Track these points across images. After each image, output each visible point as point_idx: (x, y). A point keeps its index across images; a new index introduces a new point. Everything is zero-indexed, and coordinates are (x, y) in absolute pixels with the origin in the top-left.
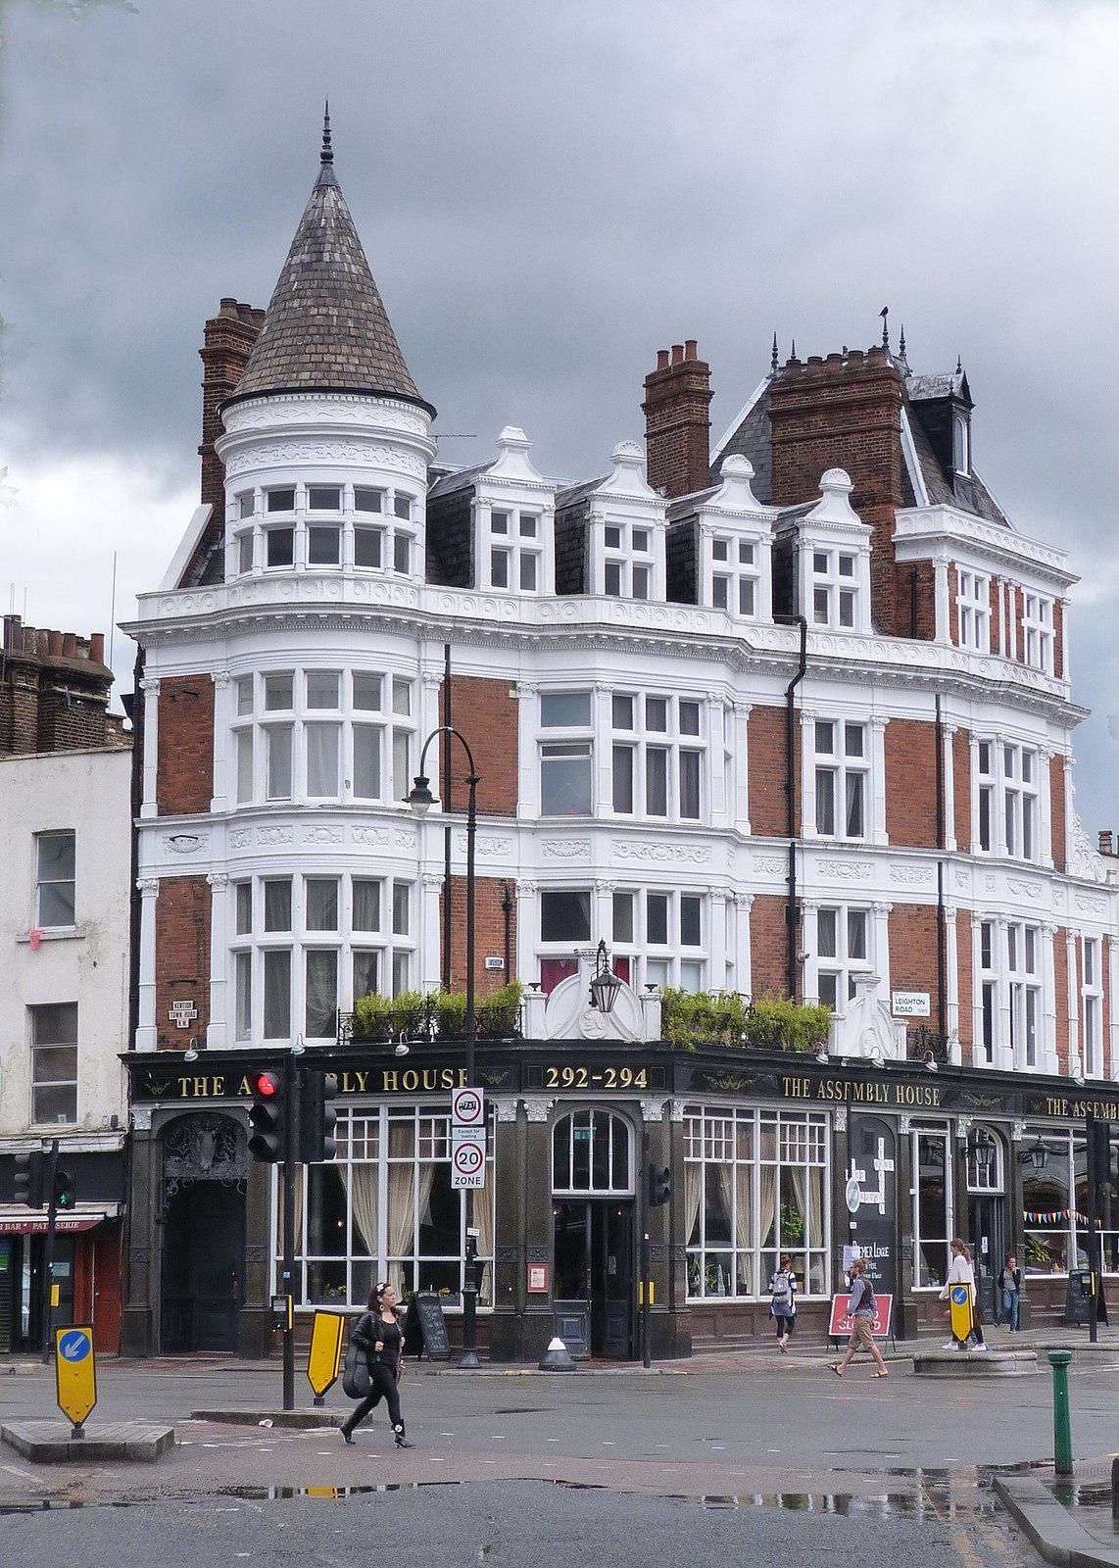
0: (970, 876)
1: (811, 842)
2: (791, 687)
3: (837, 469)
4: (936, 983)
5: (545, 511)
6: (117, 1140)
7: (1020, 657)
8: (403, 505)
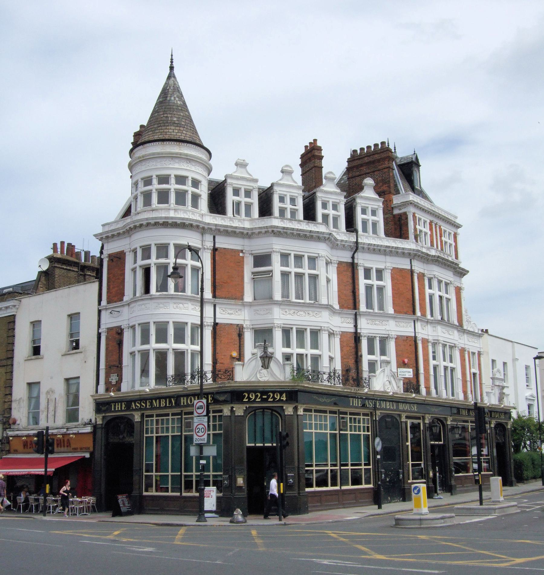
0: (426, 327)
1: (363, 312)
2: (353, 255)
3: (369, 178)
4: (415, 365)
5: (254, 188)
6: (90, 428)
7: (442, 249)
8: (293, 201)
